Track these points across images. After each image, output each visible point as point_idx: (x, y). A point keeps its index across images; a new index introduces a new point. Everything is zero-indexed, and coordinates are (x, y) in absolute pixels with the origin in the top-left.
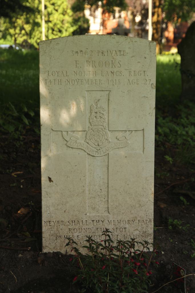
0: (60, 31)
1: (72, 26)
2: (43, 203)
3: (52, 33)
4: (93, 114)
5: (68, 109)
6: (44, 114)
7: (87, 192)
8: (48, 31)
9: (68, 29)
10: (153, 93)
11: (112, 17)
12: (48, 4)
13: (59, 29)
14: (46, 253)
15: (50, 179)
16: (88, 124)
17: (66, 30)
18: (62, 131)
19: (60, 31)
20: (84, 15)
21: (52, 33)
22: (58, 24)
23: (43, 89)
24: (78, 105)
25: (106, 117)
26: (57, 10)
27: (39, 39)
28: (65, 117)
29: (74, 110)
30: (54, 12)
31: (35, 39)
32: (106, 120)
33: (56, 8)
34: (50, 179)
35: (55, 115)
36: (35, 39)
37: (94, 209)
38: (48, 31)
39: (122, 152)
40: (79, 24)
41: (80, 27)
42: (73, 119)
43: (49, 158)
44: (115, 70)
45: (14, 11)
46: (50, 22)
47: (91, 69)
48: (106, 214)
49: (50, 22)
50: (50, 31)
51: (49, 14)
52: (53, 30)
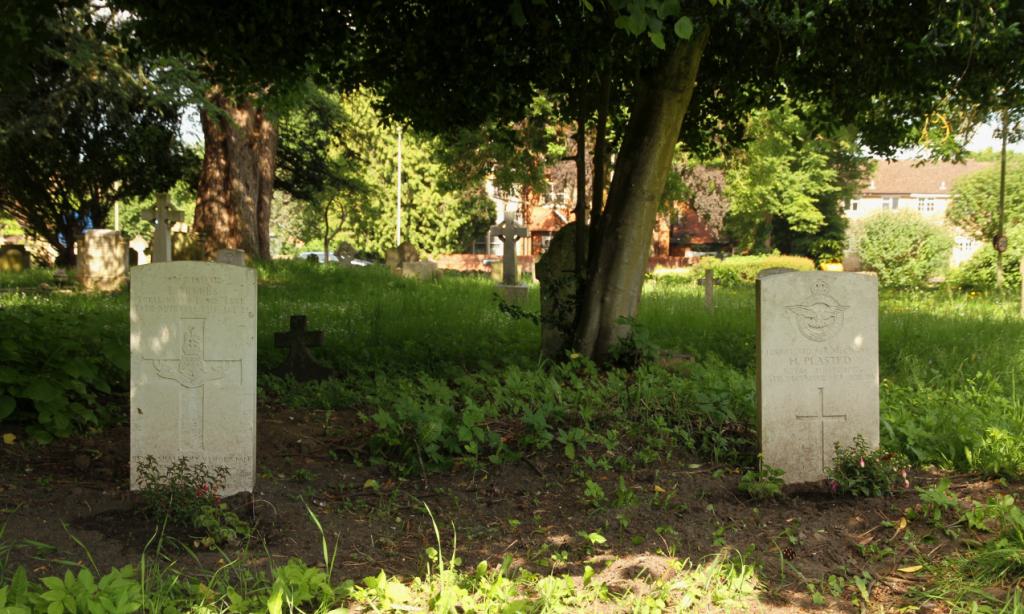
0: (434, 226)
1: (459, 217)
2: (132, 437)
3: (417, 230)
4: (187, 342)
5: (159, 336)
6: (135, 341)
7: (180, 426)
8: (408, 225)
9: (451, 222)
10: (253, 322)
11: (542, 200)
12: (410, 171)
13: (430, 221)
14: (133, 492)
15: (140, 411)
16: (181, 353)
17: (446, 225)
18: (153, 360)
19: (434, 226)
20: (484, 193)
21: (417, 230)
22: (430, 211)
23: (133, 315)
24: (170, 332)
25: (201, 345)
26: (428, 185)
27: (388, 240)
28: (156, 344)
29: (165, 336)
30: (422, 186)
31: (382, 240)
32: (201, 349)
33: (427, 180)
34: (140, 411)
35: (145, 341)
36: (382, 240)
37: (188, 444)
38: (408, 225)
39: (218, 383)
40: (474, 211)
41: (475, 217)
42: (166, 347)
43: (139, 388)
44: (210, 297)
45: (320, 188)
46: (414, 207)
47: (184, 295)
48: (201, 450)
49: (414, 207)
50: (413, 226)
51: (412, 192)
52: (420, 224)
